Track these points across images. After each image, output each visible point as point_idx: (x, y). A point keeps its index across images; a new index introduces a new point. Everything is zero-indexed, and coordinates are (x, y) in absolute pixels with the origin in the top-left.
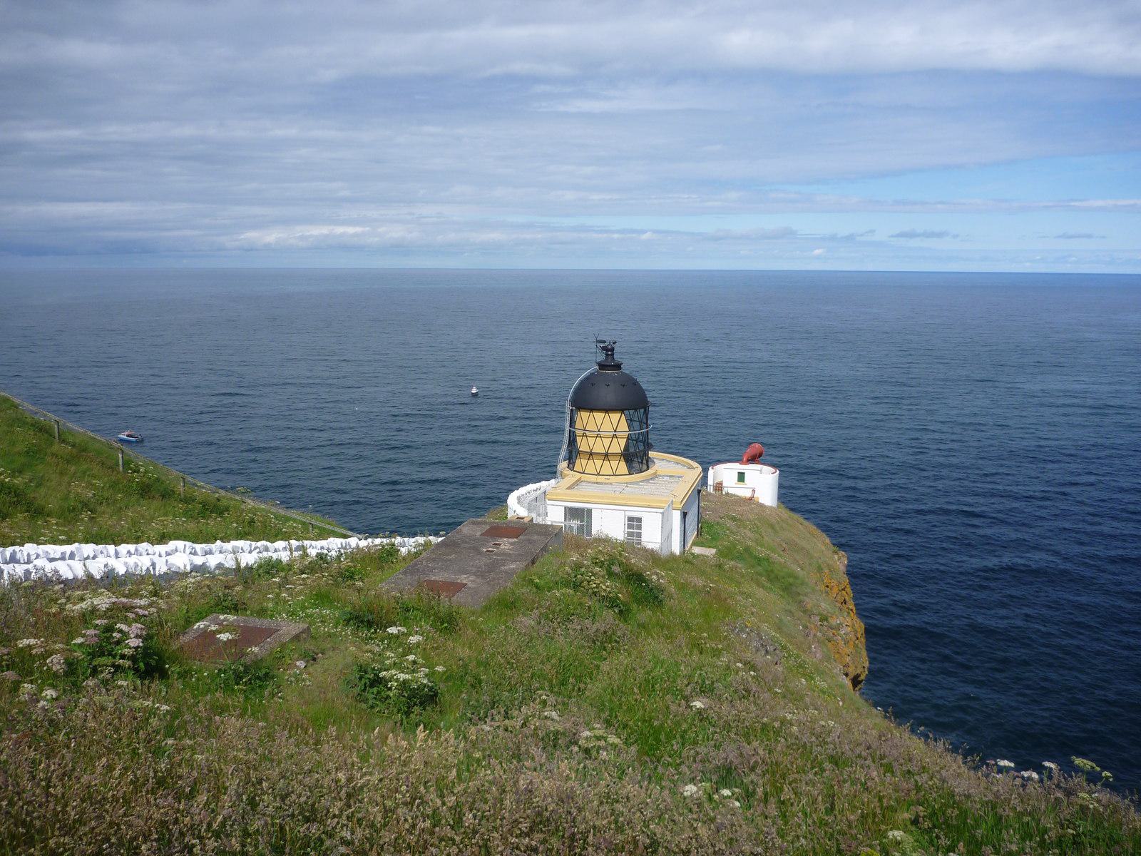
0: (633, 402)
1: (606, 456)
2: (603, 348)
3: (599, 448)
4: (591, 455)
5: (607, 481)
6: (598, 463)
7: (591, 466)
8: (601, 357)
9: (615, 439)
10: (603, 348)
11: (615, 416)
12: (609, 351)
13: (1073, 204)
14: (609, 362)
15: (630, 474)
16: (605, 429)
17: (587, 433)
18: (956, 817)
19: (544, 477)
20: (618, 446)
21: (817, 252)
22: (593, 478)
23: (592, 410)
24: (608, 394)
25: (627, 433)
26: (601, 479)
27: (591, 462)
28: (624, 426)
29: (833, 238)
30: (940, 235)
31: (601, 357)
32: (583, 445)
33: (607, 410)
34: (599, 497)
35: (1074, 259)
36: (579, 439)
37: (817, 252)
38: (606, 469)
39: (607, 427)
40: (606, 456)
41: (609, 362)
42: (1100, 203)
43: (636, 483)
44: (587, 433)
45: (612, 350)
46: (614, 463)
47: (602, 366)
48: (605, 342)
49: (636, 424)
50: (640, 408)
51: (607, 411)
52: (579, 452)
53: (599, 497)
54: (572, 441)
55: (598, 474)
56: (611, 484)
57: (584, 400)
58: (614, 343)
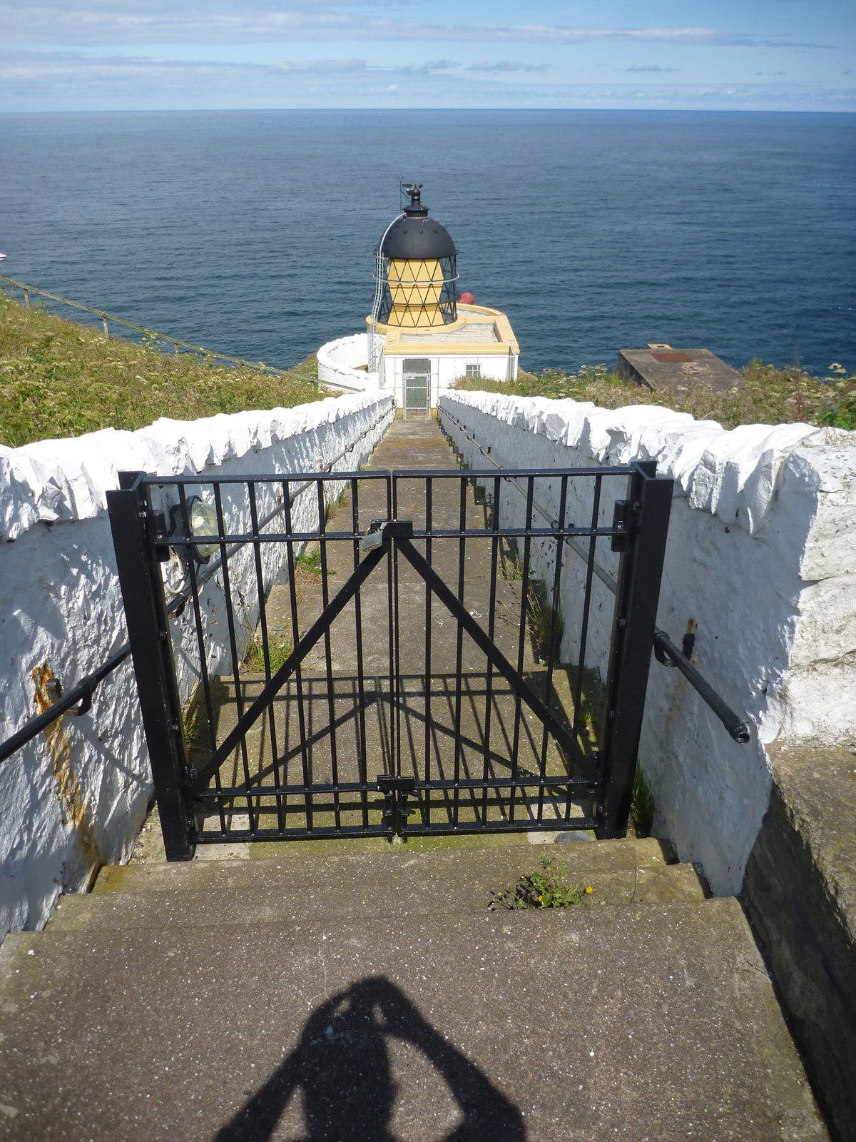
0: (444, 251)
1: (424, 307)
3: (416, 299)
4: (407, 307)
5: (427, 332)
6: (416, 314)
7: (407, 318)
8: (407, 202)
9: (431, 289)
10: (409, 193)
11: (431, 265)
12: (415, 196)
13: (631, 33)
14: (415, 210)
15: (445, 324)
16: (418, 279)
17: (433, 283)
19: (342, 324)
20: (434, 296)
21: (393, 87)
22: (413, 331)
23: (407, 259)
24: (417, 241)
25: (442, 283)
26: (421, 331)
27: (408, 314)
29: (406, 71)
30: (516, 68)
31: (407, 202)
32: (398, 297)
33: (423, 259)
35: (640, 94)
36: (393, 292)
37: (393, 87)
38: (424, 318)
39: (424, 277)
40: (424, 307)
41: (415, 210)
42: (657, 32)
43: (452, 333)
45: (418, 194)
46: (431, 314)
47: (410, 212)
48: (410, 186)
49: (448, 275)
51: (423, 259)
52: (393, 304)
53: (423, 348)
54: (386, 290)
57: (395, 250)
58: (421, 186)
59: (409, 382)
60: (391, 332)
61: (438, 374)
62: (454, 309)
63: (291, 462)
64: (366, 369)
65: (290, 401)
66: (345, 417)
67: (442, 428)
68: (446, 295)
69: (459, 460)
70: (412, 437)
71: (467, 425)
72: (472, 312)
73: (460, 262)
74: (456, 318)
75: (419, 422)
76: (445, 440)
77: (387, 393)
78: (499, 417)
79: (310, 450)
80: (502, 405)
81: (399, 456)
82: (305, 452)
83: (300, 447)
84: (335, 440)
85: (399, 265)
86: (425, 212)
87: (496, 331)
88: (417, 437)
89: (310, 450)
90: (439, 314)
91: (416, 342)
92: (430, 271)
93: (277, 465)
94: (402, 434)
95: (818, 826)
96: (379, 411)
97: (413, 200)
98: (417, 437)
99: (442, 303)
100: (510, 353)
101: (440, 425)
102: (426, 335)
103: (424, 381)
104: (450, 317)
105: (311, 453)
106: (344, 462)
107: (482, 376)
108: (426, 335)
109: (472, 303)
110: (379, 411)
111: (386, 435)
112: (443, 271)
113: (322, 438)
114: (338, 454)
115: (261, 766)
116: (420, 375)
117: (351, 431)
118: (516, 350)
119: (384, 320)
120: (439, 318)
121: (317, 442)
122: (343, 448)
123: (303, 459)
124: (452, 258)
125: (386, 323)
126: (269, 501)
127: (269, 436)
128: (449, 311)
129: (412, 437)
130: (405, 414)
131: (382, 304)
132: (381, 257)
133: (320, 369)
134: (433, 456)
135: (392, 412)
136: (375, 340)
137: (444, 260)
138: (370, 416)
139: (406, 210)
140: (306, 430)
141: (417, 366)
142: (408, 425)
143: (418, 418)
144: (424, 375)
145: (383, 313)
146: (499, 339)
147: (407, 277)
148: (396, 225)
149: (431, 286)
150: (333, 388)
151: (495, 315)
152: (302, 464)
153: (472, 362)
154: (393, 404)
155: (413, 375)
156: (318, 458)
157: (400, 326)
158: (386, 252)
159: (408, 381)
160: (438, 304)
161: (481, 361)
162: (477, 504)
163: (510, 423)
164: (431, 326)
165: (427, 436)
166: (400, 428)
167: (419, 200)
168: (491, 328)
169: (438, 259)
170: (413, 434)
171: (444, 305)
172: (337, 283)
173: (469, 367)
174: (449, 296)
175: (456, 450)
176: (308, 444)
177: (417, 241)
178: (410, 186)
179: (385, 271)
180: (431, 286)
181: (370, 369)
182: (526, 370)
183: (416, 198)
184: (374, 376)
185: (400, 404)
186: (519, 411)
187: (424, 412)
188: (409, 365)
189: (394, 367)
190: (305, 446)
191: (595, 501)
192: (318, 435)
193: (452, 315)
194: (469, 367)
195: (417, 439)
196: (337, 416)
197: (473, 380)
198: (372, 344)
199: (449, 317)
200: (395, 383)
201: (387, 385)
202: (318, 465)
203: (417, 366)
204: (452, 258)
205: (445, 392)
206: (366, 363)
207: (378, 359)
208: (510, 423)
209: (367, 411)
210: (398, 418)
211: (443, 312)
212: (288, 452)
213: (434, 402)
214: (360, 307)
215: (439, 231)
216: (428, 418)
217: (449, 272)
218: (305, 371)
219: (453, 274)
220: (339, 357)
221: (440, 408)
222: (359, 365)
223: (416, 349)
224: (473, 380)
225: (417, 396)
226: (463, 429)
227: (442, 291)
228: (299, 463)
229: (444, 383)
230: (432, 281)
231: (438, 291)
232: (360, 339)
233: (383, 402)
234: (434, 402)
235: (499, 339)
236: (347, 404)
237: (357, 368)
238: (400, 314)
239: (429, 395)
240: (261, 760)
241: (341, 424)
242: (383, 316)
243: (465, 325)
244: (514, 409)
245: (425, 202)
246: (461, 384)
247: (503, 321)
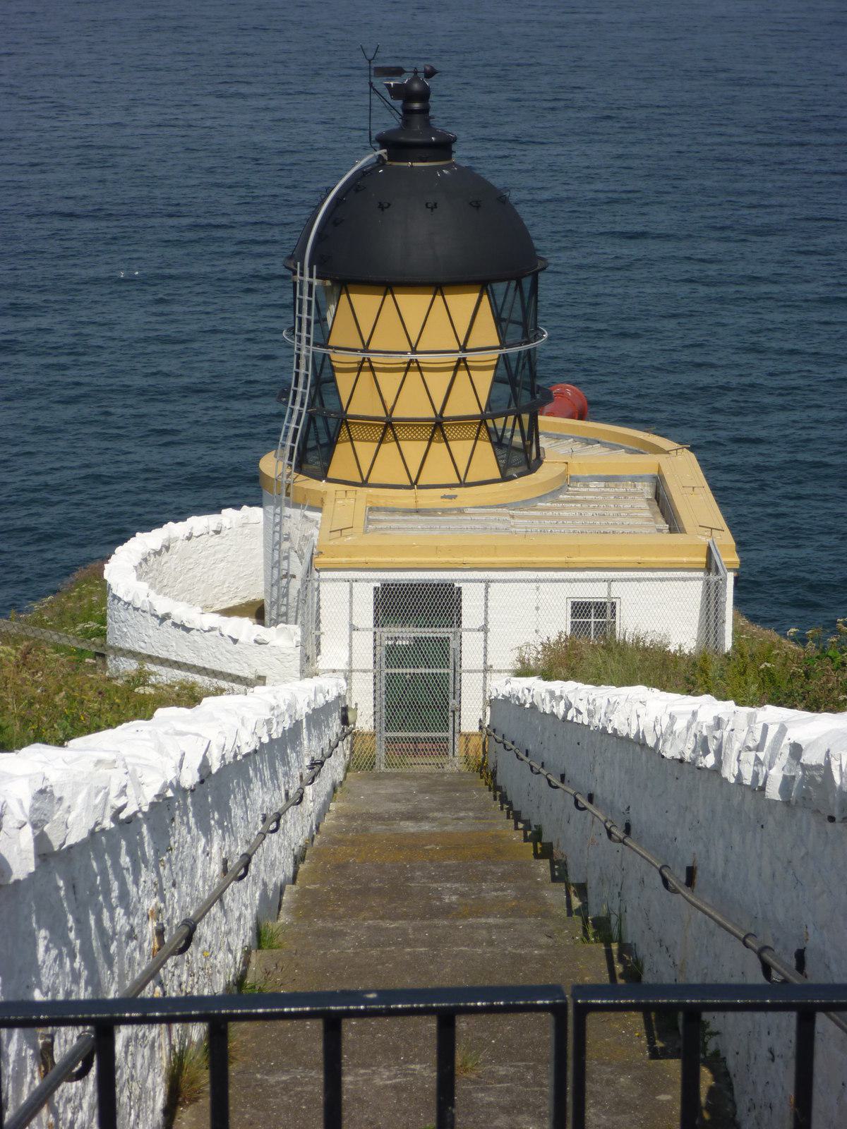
0: (497, 260)
1: (438, 427)
2: (396, 92)
3: (414, 405)
4: (389, 427)
5: (448, 504)
6: (414, 450)
7: (388, 463)
9: (462, 375)
10: (396, 92)
11: (463, 303)
12: (413, 99)
14: (415, 137)
15: (505, 478)
17: (374, 357)
18: (592, 920)
20: (473, 392)
22: (406, 498)
23: (388, 285)
24: (418, 232)
25: (494, 355)
27: (389, 449)
28: (486, 333)
31: (388, 121)
32: (360, 397)
33: (438, 285)
34: (450, 550)
36: (344, 382)
38: (439, 467)
39: (439, 337)
40: (438, 427)
41: (415, 137)
43: (527, 504)
44: (374, 357)
45: (424, 96)
46: (461, 448)
47: (395, 147)
48: (399, 72)
49: (515, 331)
50: (512, 279)
52: (343, 419)
53: (437, 550)
54: (324, 379)
55: (413, 485)
56: (461, 511)
57: (353, 257)
58: (430, 74)
59: (392, 655)
60: (344, 504)
61: (484, 629)
62: (532, 433)
63: (77, 921)
64: (258, 613)
65: (62, 722)
66: (224, 768)
67: (504, 799)
68: (507, 389)
69: (576, 903)
70: (410, 827)
71: (598, 791)
72: (588, 442)
73: (549, 290)
74: (539, 461)
75: (425, 776)
76: (517, 836)
77: (331, 687)
78: (729, 773)
79: (129, 879)
80: (741, 736)
81: (379, 892)
82: (115, 885)
83: (104, 872)
84: (195, 840)
85: (366, 303)
86: (443, 148)
87: (662, 501)
88: (426, 827)
89: (129, 879)
90: (485, 449)
91: (415, 533)
92: (461, 320)
93: (43, 933)
94: (378, 818)
96: (310, 746)
97: (408, 112)
98: (426, 827)
99: (493, 417)
100: (710, 566)
101: (496, 788)
102: (445, 511)
103: (443, 652)
104: (519, 458)
105: (132, 889)
106: (220, 914)
107: (619, 636)
108: (445, 511)
109: (581, 417)
110: (310, 746)
111: (328, 821)
112: (498, 320)
113: (163, 846)
114: (204, 892)
117: (237, 812)
118: (729, 557)
119: (316, 466)
120: (486, 461)
121: (150, 852)
122: (216, 868)
123: (112, 910)
124: (527, 283)
125: (322, 475)
126: (19, 1051)
127: (26, 838)
128: (518, 439)
129: (410, 827)
130: (381, 753)
131: (311, 419)
132: (308, 278)
133: (116, 614)
134: (489, 891)
135: (344, 747)
136: (288, 526)
137: (500, 287)
138: (286, 762)
139: (383, 141)
140: (123, 816)
141: (419, 611)
142: (388, 788)
143: (423, 765)
145: (311, 444)
146: (673, 522)
147: (388, 338)
148: (354, 186)
149: (461, 365)
150: (166, 676)
151: (658, 450)
152: (107, 923)
153: (593, 592)
154: (345, 721)
155: (405, 634)
156: (150, 903)
157: (364, 483)
158: (322, 262)
159: (390, 650)
160: (482, 419)
161: (618, 590)
162: (655, 1054)
163: (773, 792)
164: (463, 484)
165: (459, 823)
166: (376, 796)
167: (425, 111)
168: (647, 489)
169: (482, 284)
170: (412, 816)
171: (500, 422)
172: (591, 304)
173: (580, 609)
174: (515, 396)
175: (560, 874)
176: (125, 860)
177: (418, 232)
178: (399, 72)
179: (321, 320)
180: (461, 365)
181: (270, 613)
182: (754, 619)
183: (416, 106)
184: (283, 639)
185: (364, 721)
186: (812, 757)
187: (441, 747)
188: (395, 603)
189: (347, 606)
190: (116, 862)
192: (152, 830)
193: (526, 450)
194: (580, 609)
195: (431, 837)
196: (204, 766)
197: (592, 648)
198: (277, 541)
199: (518, 457)
200: (347, 655)
201: (323, 662)
202: (151, 926)
203: (419, 611)
204: (527, 283)
205: (503, 685)
206: (257, 592)
207: (296, 585)
208: (773, 792)
209: (275, 750)
210: (360, 765)
211: (499, 443)
212: (73, 887)
213: (472, 715)
214: (249, 429)
215: (487, 205)
216: (455, 763)
217: (516, 322)
218: (64, 619)
219: (529, 331)
220: (173, 577)
221: (489, 732)
222: (236, 602)
223: (416, 555)
224: (592, 648)
225: (417, 691)
226: (584, 802)
227: (496, 380)
228: (99, 921)
229: (504, 658)
230: (414, 351)
231: (484, 380)
232: (242, 525)
233: (317, 717)
234: (472, 715)
235: (673, 522)
236: (221, 728)
237: (228, 612)
238: (365, 450)
239: (457, 694)
240: (351, 619)
241: (213, 790)
242: (313, 456)
243: (567, 481)
244: (785, 752)
246: (562, 661)
247: (683, 471)
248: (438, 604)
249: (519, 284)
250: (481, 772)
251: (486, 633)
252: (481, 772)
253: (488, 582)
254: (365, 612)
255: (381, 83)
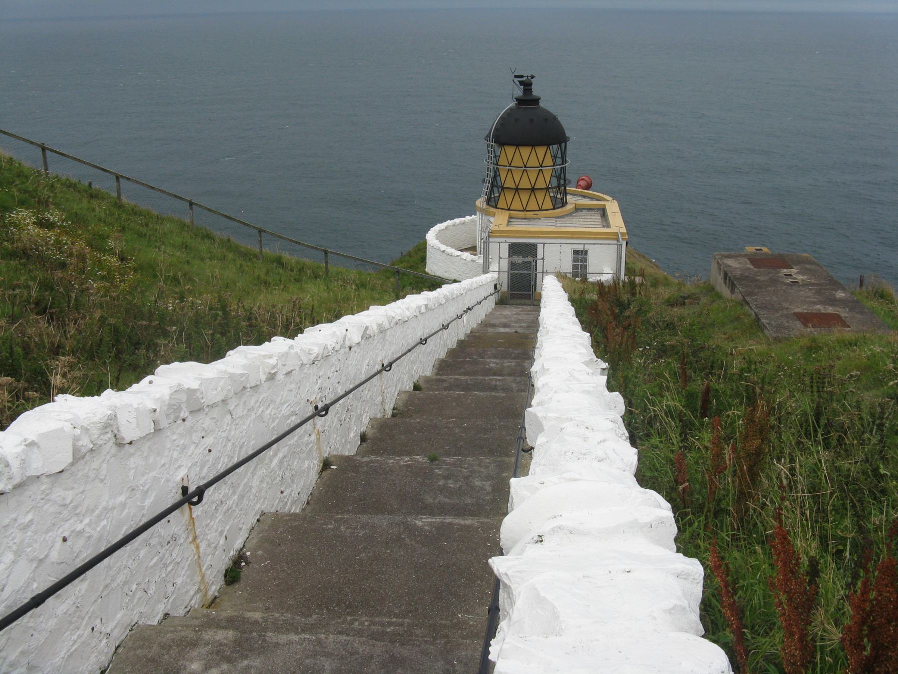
2: (521, 83)
8: (519, 92)
12: (527, 85)
14: (528, 100)
15: (554, 208)
22: (521, 214)
28: (548, 161)
41: (528, 100)
45: (530, 84)
48: (522, 76)
59: (512, 266)
61: (543, 259)
85: (510, 150)
95: (746, 563)
115: (196, 204)
116: (525, 260)
129: (502, 330)
144: (530, 259)
155: (519, 260)
157: (509, 209)
161: (587, 247)
164: (540, 210)
170: (505, 326)
188: (515, 249)
189: (500, 251)
191: (134, 538)
194: (576, 252)
204: (563, 145)
240: (200, 206)
245: (536, 91)
248: (530, 250)
249: (560, 146)
250: (856, 576)
251: (265, 231)
252: (856, 576)
253: (544, 244)
254: (505, 252)
255: (516, 80)
